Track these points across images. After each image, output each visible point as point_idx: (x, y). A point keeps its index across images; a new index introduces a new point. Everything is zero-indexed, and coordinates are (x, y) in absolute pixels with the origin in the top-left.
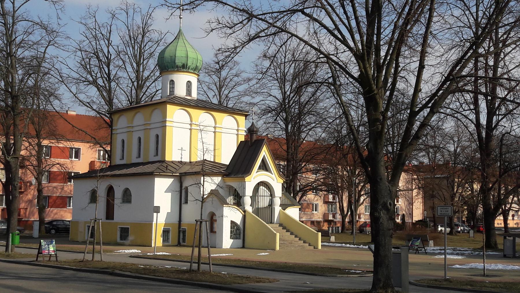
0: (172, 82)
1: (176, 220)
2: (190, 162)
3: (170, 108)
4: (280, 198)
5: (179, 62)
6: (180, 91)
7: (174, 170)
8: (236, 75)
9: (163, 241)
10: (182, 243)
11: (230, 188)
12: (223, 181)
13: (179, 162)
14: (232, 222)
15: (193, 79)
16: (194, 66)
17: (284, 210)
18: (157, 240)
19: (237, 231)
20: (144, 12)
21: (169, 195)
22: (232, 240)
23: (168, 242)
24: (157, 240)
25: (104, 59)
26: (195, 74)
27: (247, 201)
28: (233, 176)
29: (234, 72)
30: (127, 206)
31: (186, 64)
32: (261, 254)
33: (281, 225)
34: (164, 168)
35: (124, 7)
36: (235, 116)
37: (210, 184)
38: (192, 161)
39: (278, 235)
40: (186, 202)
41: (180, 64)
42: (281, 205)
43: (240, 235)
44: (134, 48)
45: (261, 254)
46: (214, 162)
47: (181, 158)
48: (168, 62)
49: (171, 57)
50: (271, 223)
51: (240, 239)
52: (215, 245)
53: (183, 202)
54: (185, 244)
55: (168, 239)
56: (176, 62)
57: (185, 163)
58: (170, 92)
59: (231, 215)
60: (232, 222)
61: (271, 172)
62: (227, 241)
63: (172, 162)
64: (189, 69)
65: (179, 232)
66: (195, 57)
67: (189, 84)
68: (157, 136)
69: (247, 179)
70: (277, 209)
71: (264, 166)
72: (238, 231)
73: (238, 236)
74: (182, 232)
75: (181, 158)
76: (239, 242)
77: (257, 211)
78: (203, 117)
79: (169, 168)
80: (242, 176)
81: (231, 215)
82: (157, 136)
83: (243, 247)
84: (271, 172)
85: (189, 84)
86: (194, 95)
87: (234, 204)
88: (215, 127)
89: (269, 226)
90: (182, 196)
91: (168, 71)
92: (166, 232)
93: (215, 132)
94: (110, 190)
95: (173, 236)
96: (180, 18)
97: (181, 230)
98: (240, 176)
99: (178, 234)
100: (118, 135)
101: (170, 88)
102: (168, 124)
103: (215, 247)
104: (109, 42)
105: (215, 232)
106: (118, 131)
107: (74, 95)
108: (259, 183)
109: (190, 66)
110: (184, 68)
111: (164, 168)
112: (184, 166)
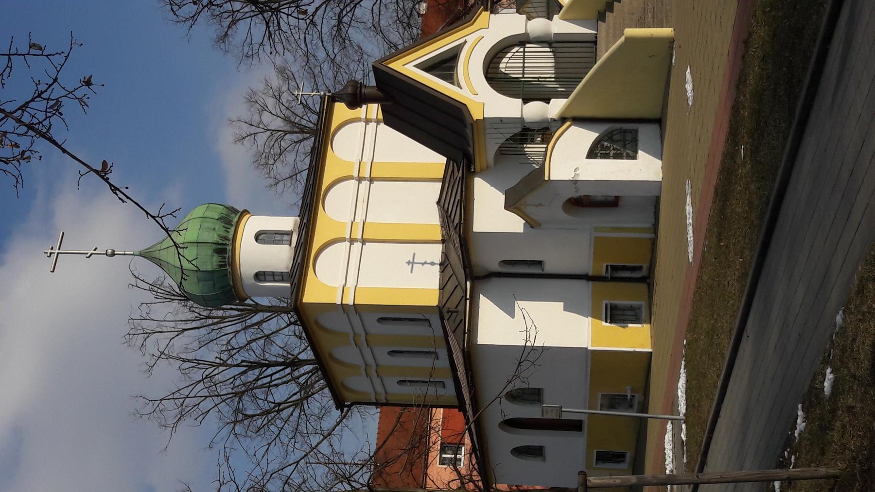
0: (260, 276)
1: (583, 288)
2: (443, 241)
3: (311, 295)
4: (529, 18)
5: (209, 262)
6: (280, 257)
7: (459, 293)
8: (278, 98)
9: (637, 320)
10: (644, 272)
11: (502, 152)
12: (484, 173)
13: (442, 271)
14: (592, 154)
15: (251, 225)
16: (219, 226)
17: (561, 7)
18: (635, 338)
19: (616, 141)
20: (150, 297)
21: (520, 304)
22: (640, 153)
23: (639, 308)
24: (635, 338)
25: (252, 375)
26: (238, 223)
27: (535, 111)
28: (471, 149)
29: (271, 102)
30: (546, 396)
31: (214, 246)
32: (690, 94)
33: (601, 17)
34: (452, 317)
35: (140, 339)
36: (334, 126)
37: (491, 211)
38: (440, 238)
39: (630, 32)
40: (540, 263)
41: (216, 259)
42: (550, 18)
43: (625, 131)
44: (222, 319)
45: (690, 94)
46: (443, 181)
47: (433, 264)
48: (214, 286)
49: (199, 280)
50: (595, 43)
51: (636, 132)
52: (650, 200)
53: (540, 272)
54: (645, 266)
55: (632, 308)
56: (209, 268)
57: (445, 255)
58: (283, 281)
59: (570, 158)
60: (592, 154)
61: (460, 47)
62: (643, 168)
63: (442, 288)
64: (226, 238)
65: (614, 279)
66: (197, 223)
67: (260, 237)
68: (382, 320)
69: (477, 115)
70: (559, 26)
71: (445, 66)
72: (615, 138)
73: (629, 137)
74: (615, 275)
75: (433, 264)
76: (646, 133)
77: (566, 80)
78: (337, 208)
79: (451, 305)
80: (469, 127)
81: (570, 158)
82: (382, 320)
83: (659, 122)
84: (460, 47)
85: (260, 237)
86: (288, 223)
87: (546, 140)
88: (360, 179)
89: (603, 58)
90: (521, 274)
91: (235, 286)
92: (617, 315)
93: (371, 180)
94: (513, 424)
95: (626, 296)
96: (113, 254)
97: (609, 275)
98: (468, 131)
99: (620, 284)
100: (389, 390)
101: (274, 281)
102: (349, 300)
103: (658, 199)
104: (220, 365)
105: (617, 198)
106: (379, 388)
107: (325, 437)
108: (486, 77)
109: (219, 236)
110: (225, 250)
111: (452, 317)
112: (451, 260)
